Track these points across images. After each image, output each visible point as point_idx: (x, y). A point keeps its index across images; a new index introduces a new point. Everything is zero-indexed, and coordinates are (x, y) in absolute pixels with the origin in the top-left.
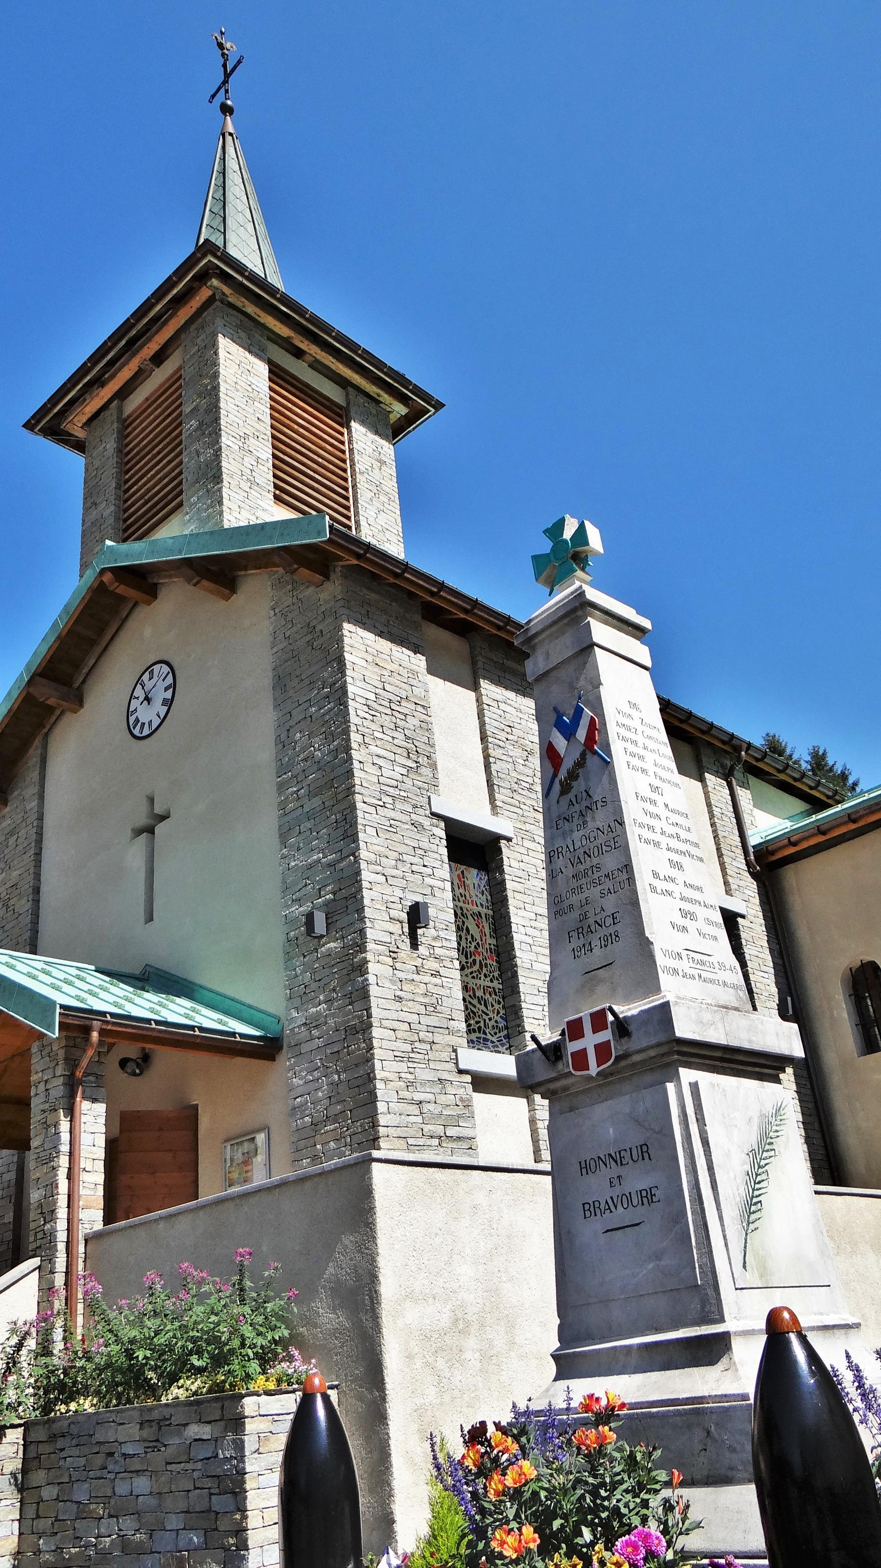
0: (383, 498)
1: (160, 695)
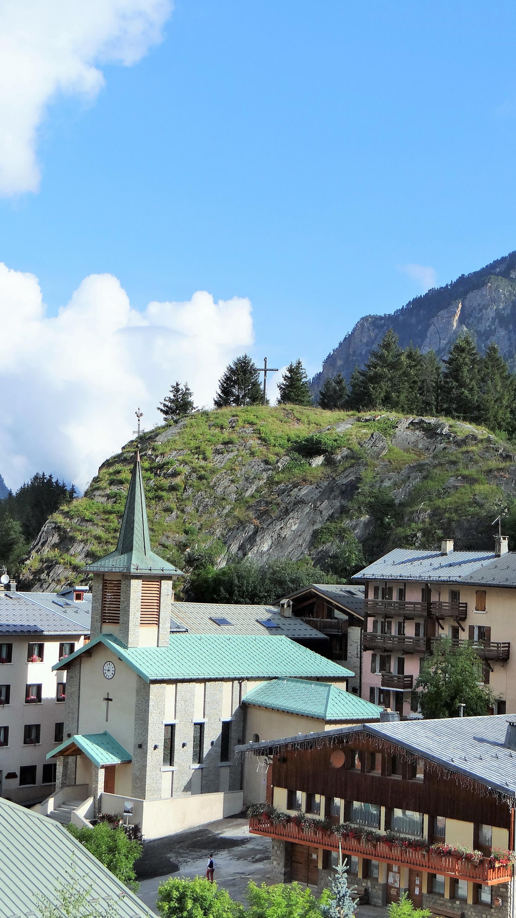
0: (167, 607)
1: (111, 672)
